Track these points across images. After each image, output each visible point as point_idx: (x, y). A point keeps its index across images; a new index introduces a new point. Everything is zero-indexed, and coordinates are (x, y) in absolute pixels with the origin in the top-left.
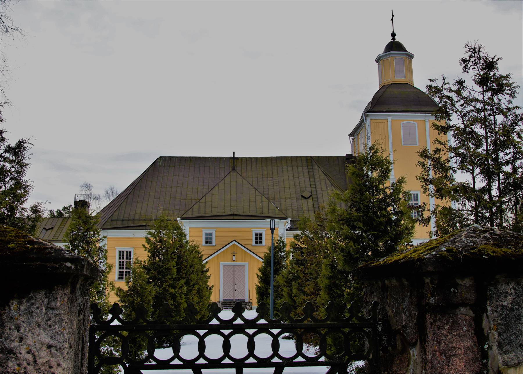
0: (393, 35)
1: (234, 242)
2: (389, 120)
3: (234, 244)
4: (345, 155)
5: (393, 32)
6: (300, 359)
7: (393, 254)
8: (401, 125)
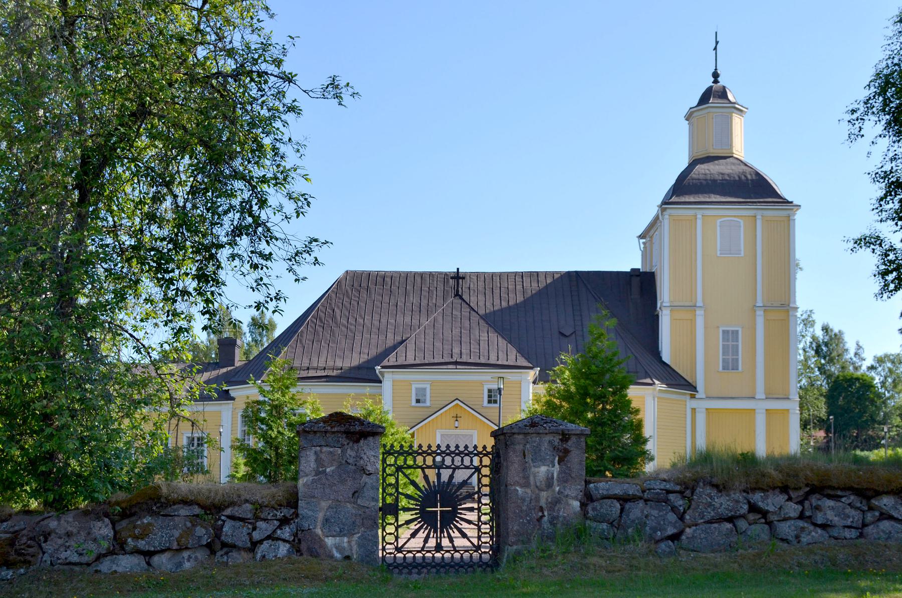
0: (716, 75)
1: (457, 402)
2: (699, 216)
3: (457, 405)
4: (629, 270)
5: (716, 69)
6: (462, 466)
7: (621, 455)
8: (718, 224)
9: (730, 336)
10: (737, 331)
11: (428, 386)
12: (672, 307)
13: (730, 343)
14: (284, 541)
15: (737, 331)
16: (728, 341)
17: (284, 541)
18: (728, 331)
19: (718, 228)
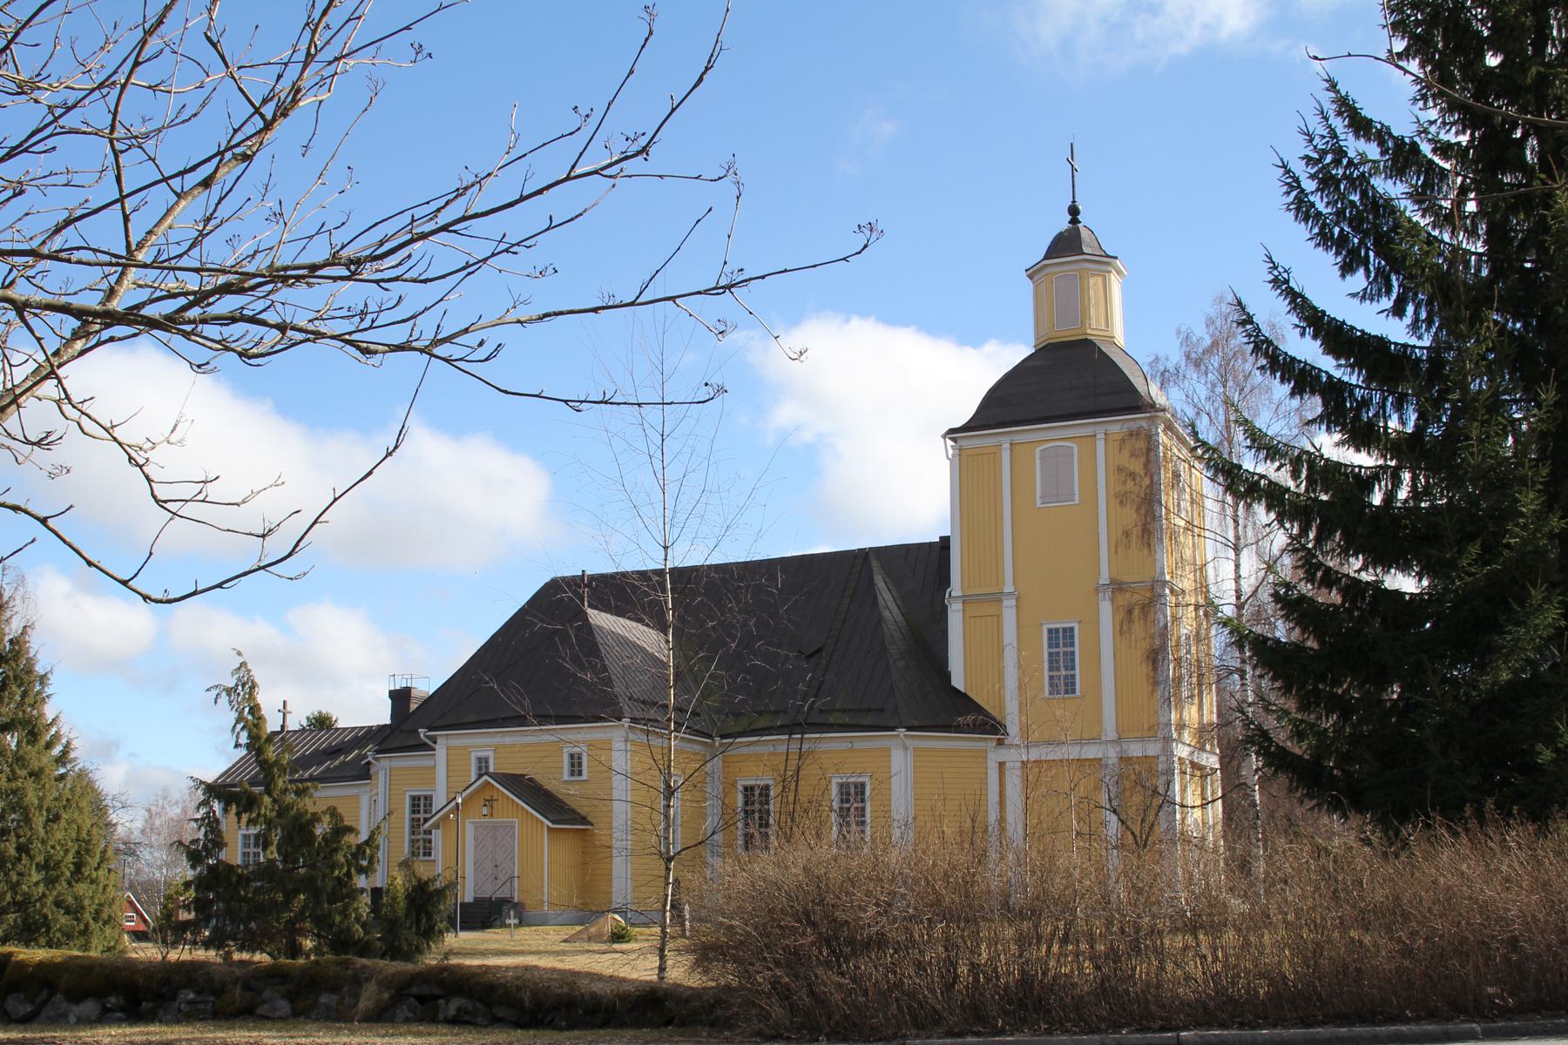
0: (1074, 211)
5: (1074, 202)
9: (1061, 638)
10: (1072, 629)
11: (491, 755)
12: (966, 600)
13: (1061, 650)
14: (662, 969)
15: (1072, 629)
16: (1057, 646)
17: (662, 969)
18: (1057, 630)
19: (1038, 462)
